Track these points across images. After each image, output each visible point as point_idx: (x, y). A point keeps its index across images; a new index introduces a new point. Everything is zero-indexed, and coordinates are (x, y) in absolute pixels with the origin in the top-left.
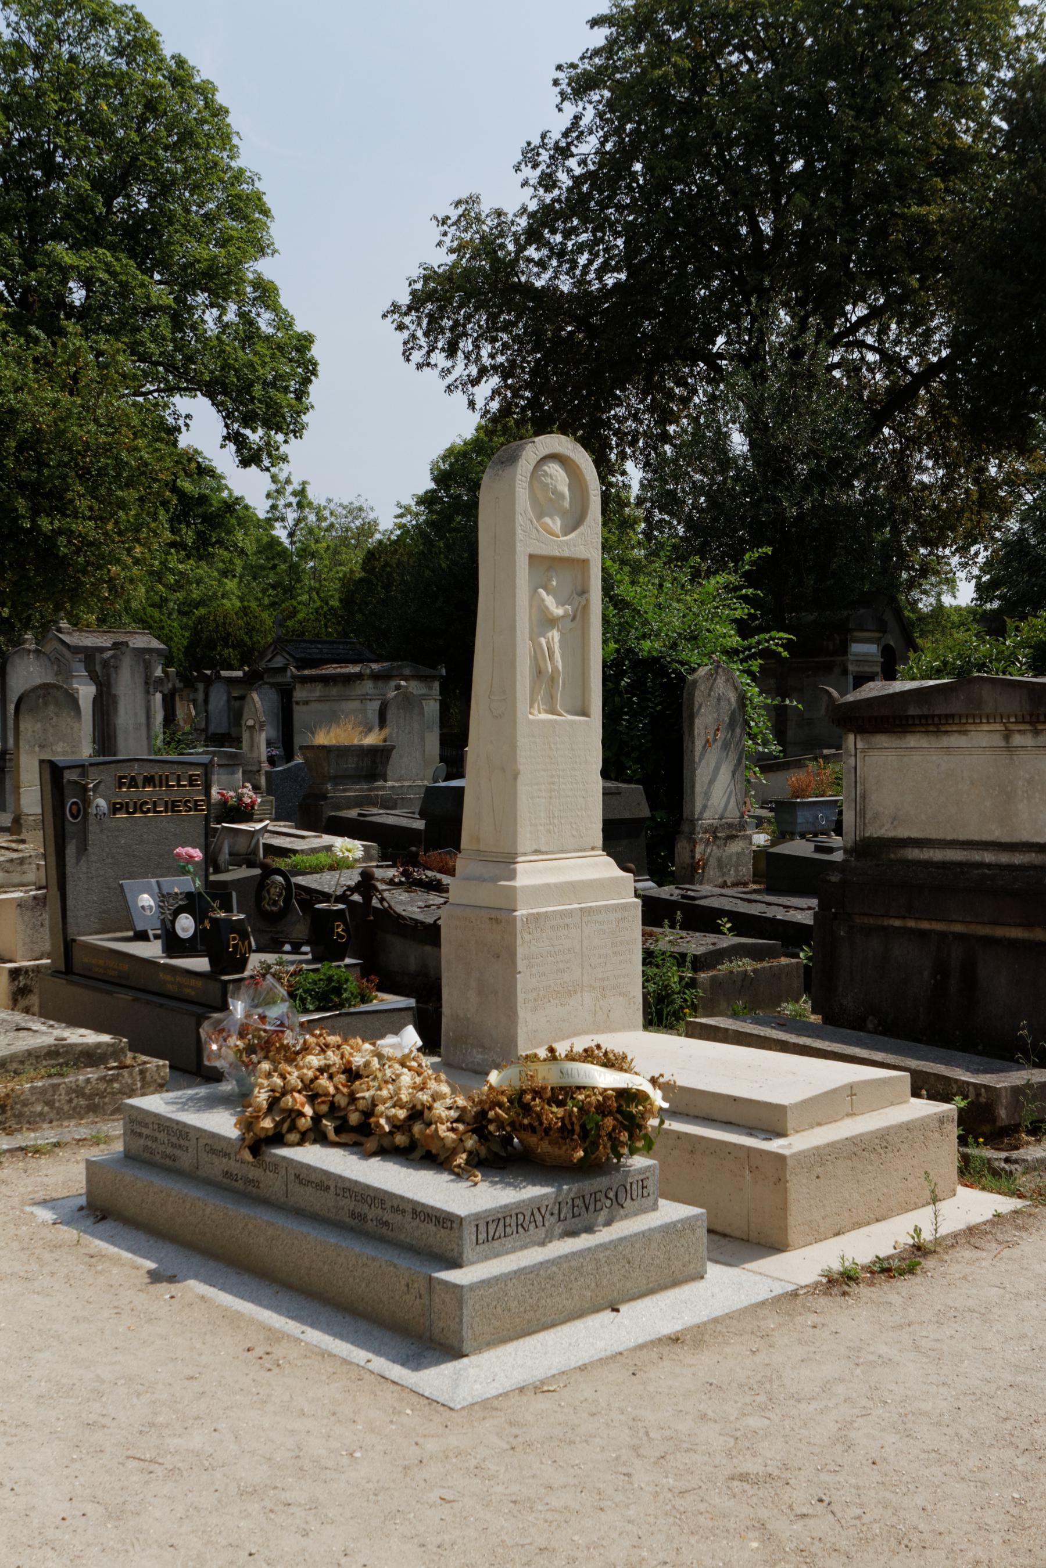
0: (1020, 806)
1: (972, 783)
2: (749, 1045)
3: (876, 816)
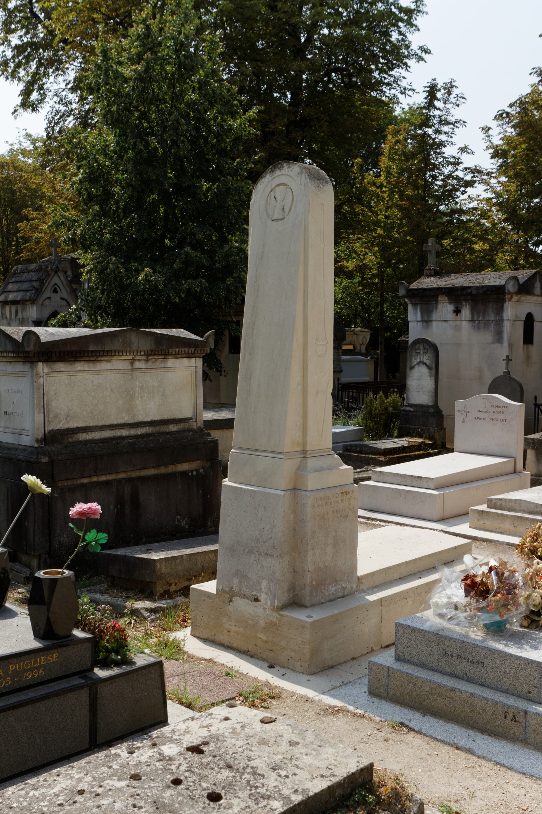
0: (137, 402)
1: (112, 391)
3: (56, 416)
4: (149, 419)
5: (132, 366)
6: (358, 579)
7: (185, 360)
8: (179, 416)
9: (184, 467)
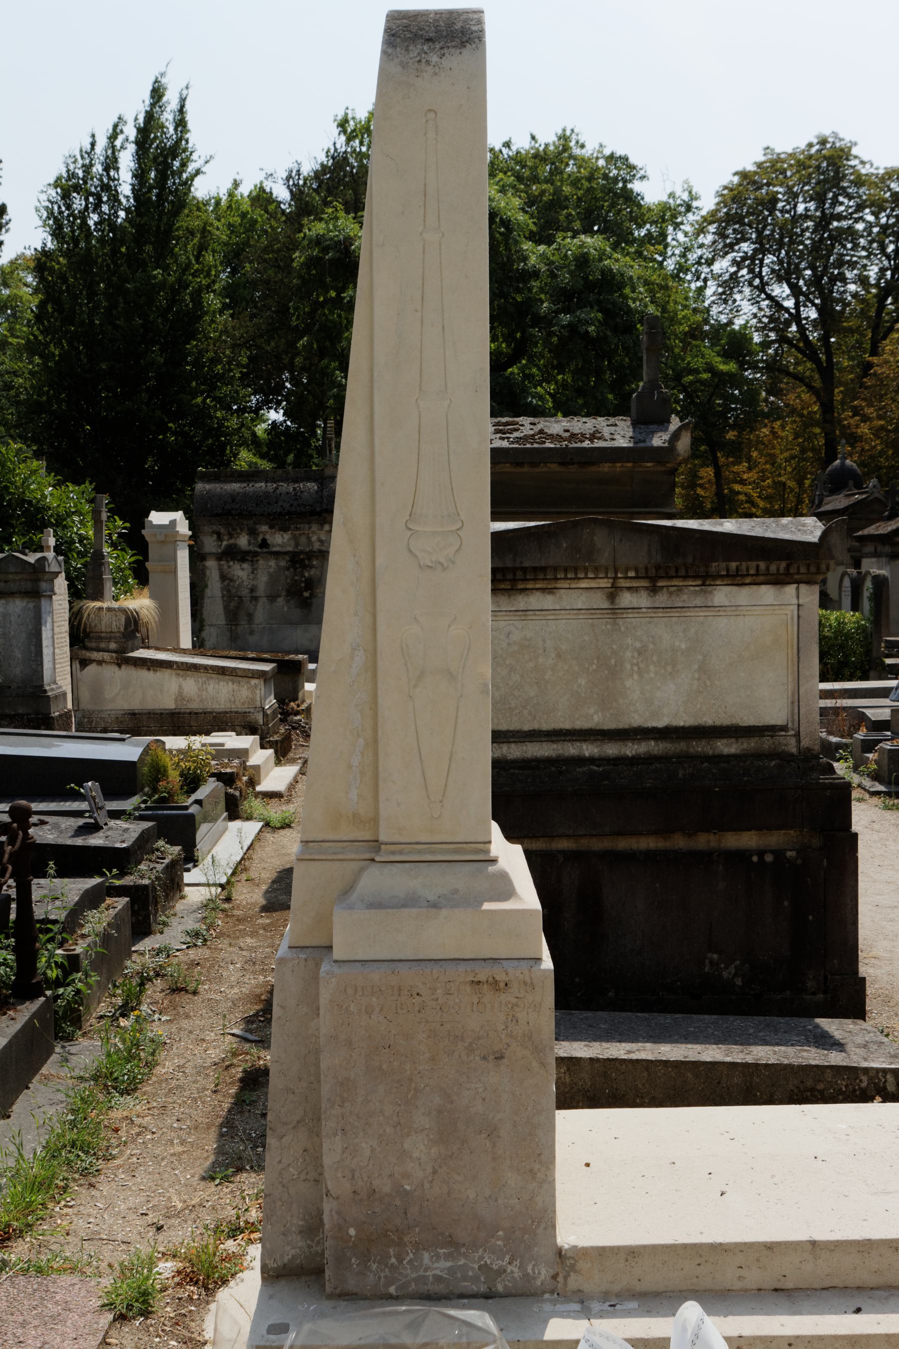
0: (628, 683)
1: (559, 656)
2: (864, 1097)
4: (661, 723)
5: (613, 602)
6: (560, 1253)
7: (767, 593)
8: (748, 720)
9: (748, 840)
